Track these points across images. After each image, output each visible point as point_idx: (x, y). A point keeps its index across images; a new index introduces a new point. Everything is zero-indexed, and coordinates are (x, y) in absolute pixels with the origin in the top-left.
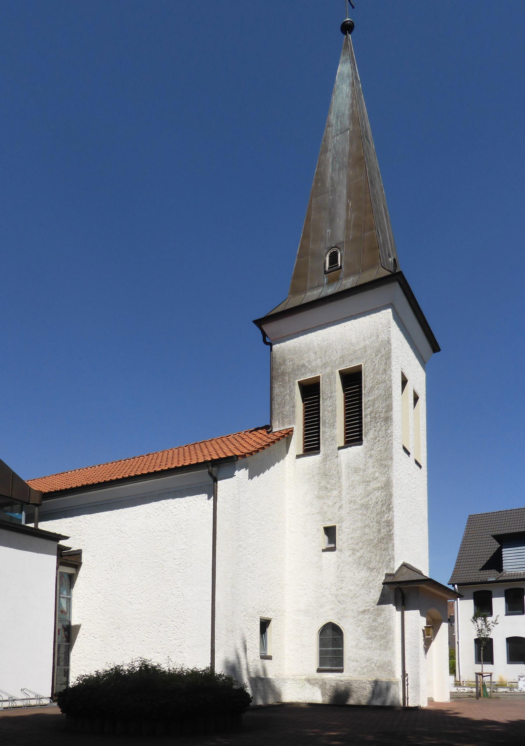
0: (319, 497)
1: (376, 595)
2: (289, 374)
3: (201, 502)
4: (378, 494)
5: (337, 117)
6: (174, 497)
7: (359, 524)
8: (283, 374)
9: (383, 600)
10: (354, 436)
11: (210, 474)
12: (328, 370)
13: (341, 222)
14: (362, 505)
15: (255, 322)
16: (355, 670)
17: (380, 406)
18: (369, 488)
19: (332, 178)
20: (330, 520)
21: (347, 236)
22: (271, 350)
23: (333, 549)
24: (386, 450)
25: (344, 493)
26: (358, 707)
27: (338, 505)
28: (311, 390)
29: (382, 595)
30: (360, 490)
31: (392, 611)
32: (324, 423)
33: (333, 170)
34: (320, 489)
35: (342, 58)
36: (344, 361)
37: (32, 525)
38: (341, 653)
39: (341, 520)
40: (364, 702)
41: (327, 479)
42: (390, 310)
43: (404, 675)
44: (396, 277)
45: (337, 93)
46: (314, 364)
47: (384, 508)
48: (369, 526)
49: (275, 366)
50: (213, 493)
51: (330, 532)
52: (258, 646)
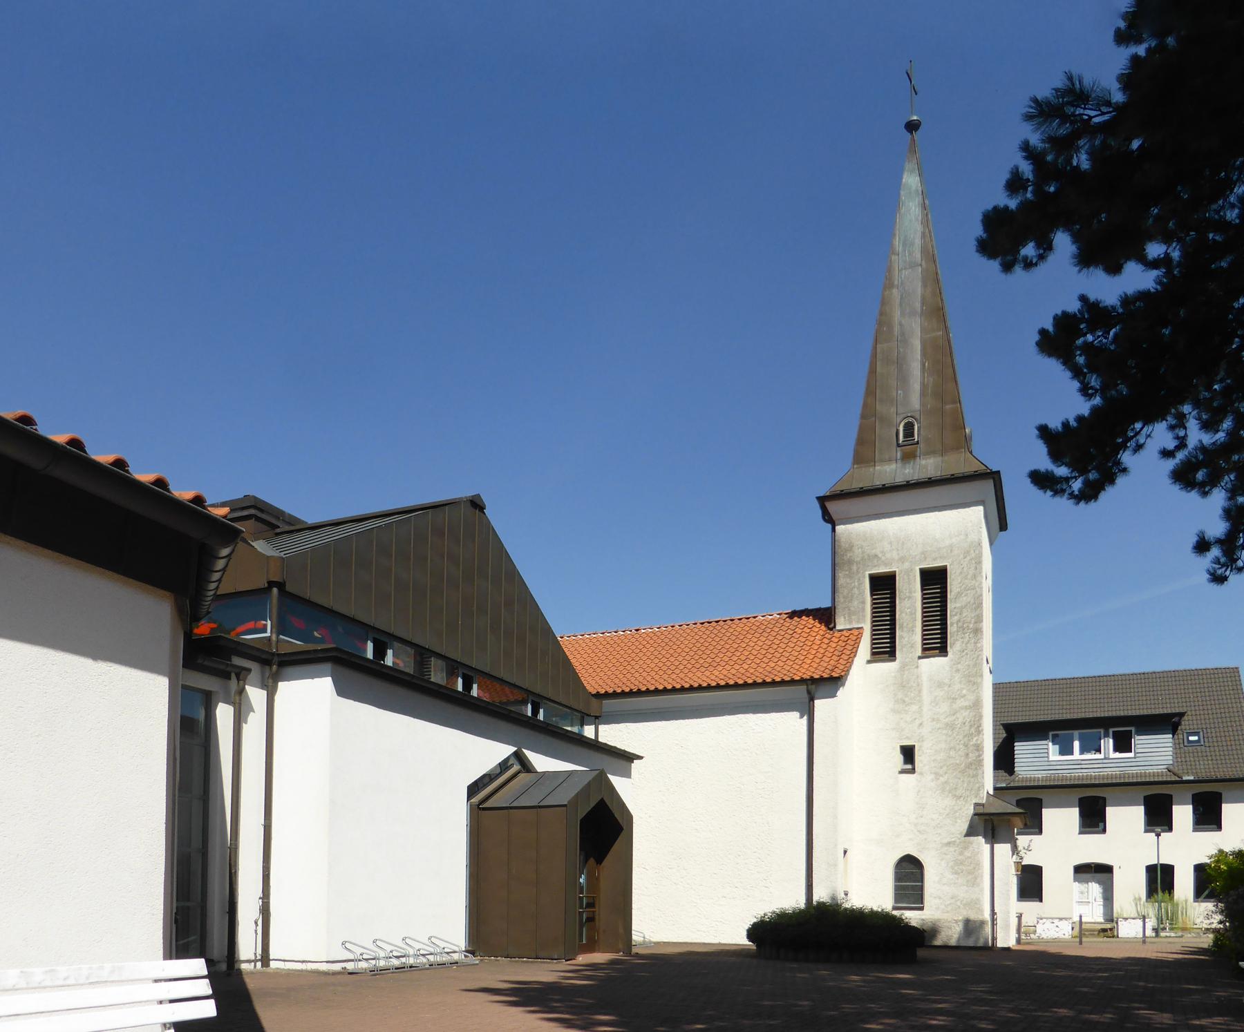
0: (894, 711)
1: (964, 826)
2: (858, 563)
3: (793, 722)
4: (965, 713)
5: (904, 244)
6: (754, 712)
7: (943, 746)
8: (850, 562)
9: (971, 832)
10: (936, 643)
11: (809, 692)
13: (916, 387)
14: (947, 724)
15: (819, 498)
16: (938, 908)
17: (968, 615)
18: (955, 706)
19: (901, 324)
21: (923, 404)
22: (834, 530)
23: (913, 771)
24: (975, 665)
25: (925, 709)
26: (946, 947)
27: (917, 722)
28: (884, 585)
30: (944, 708)
32: (901, 627)
33: (903, 314)
34: (897, 701)
35: (908, 166)
36: (925, 558)
37: (575, 729)
38: (922, 888)
39: (922, 740)
40: (953, 942)
41: (905, 691)
42: (981, 508)
43: (993, 913)
44: (995, 476)
45: (903, 211)
46: (888, 555)
47: (973, 730)
50: (1158, 835)
51: (908, 753)
52: (1100, 901)
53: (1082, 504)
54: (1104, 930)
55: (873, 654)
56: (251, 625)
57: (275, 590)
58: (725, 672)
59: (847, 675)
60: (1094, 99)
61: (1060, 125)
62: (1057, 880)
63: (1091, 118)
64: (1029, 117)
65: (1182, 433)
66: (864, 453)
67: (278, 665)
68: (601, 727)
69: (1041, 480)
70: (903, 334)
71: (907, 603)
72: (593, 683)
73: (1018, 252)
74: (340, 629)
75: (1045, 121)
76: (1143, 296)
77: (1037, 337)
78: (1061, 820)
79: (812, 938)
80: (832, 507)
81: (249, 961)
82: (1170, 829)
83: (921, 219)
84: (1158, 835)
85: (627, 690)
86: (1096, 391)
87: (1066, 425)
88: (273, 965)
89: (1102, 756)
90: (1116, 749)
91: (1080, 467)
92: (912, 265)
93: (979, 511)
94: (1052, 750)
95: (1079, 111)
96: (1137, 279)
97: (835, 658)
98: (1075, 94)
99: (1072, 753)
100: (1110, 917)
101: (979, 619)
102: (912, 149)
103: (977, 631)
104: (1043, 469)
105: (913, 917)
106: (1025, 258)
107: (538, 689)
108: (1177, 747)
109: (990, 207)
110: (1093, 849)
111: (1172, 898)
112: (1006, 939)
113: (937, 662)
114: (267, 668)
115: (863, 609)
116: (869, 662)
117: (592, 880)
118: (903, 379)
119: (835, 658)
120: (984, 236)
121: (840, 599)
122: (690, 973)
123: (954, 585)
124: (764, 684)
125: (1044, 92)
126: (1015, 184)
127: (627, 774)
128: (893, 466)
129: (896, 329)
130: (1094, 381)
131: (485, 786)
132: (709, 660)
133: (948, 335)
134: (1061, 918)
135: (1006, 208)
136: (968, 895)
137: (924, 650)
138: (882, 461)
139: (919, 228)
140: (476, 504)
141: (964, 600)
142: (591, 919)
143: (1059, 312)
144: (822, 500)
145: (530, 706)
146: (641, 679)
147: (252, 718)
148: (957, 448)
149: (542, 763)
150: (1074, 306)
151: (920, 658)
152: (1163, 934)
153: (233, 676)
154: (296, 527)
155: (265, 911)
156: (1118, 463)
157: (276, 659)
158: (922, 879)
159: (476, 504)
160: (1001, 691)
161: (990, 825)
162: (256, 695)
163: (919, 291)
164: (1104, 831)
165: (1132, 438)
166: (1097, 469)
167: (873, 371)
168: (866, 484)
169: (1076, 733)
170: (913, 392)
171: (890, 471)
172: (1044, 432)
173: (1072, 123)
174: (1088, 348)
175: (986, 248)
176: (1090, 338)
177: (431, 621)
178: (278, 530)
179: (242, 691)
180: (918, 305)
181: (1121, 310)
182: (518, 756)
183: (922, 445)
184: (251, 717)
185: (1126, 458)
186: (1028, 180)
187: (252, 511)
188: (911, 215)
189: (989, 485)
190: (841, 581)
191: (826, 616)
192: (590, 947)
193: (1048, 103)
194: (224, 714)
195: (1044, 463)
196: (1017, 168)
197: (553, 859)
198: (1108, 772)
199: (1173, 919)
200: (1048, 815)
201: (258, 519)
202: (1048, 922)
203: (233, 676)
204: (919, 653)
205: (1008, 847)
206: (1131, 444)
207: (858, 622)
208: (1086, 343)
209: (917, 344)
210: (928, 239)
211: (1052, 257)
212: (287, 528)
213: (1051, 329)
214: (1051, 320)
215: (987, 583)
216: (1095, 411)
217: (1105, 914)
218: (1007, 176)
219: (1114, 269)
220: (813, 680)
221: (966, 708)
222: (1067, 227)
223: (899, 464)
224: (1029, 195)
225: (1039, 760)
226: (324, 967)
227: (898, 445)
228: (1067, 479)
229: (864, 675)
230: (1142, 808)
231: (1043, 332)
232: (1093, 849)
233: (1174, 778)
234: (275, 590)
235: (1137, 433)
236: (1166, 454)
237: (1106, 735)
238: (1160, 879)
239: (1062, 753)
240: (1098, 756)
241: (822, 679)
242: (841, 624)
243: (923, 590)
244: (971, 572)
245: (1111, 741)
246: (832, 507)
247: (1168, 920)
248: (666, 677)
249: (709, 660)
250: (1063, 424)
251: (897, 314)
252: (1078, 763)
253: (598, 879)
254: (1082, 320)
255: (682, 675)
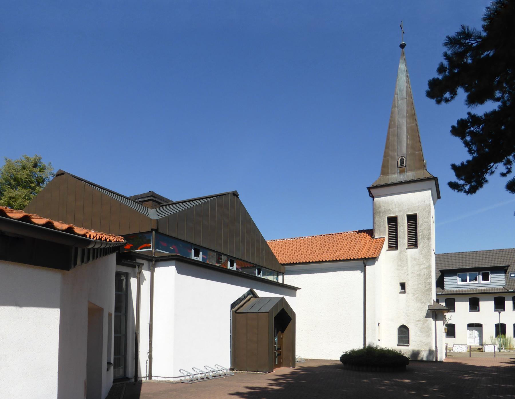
1: (425, 314)
2: (383, 213)
3: (358, 275)
5: (400, 91)
6: (343, 271)
7: (416, 283)
8: (380, 212)
9: (427, 316)
10: (413, 243)
11: (364, 263)
12: (401, 213)
13: (405, 144)
15: (367, 188)
17: (426, 232)
18: (421, 268)
19: (399, 121)
20: (402, 280)
21: (407, 151)
22: (373, 200)
23: (405, 292)
24: (428, 252)
27: (406, 274)
29: (427, 314)
30: (417, 268)
31: (431, 320)
32: (400, 237)
33: (399, 117)
35: (401, 61)
38: (408, 338)
39: (408, 280)
41: (402, 262)
42: (430, 191)
43: (436, 348)
44: (435, 179)
46: (394, 210)
47: (428, 277)
48: (420, 284)
49: (375, 208)
50: (500, 313)
51: (403, 286)
52: (478, 338)
53: (469, 195)
54: (479, 349)
55: (389, 247)
56: (145, 245)
57: (154, 232)
58: (332, 255)
59: (378, 257)
60: (474, 36)
61: (459, 48)
62: (461, 329)
63: (472, 44)
64: (446, 45)
65: (509, 167)
66: (385, 170)
67: (155, 261)
68: (285, 276)
69: (453, 186)
70: (399, 125)
71: (402, 228)
72: (282, 259)
73: (443, 96)
74: (181, 245)
75: (452, 46)
76: (494, 112)
77: (451, 129)
78: (462, 307)
79: (366, 362)
80: (373, 191)
81: (144, 377)
82: (504, 310)
83: (406, 82)
84: (500, 313)
85: (295, 262)
86: (475, 151)
87: (462, 164)
88: (153, 378)
89: (477, 282)
90: (483, 279)
91: (468, 181)
92: (403, 99)
93: (429, 192)
94: (459, 280)
95: (467, 41)
96: (490, 106)
97: (374, 249)
98: (465, 34)
99: (466, 281)
100: (481, 344)
101: (430, 234)
102: (403, 55)
103: (429, 239)
104: (453, 181)
105: (406, 351)
106: (446, 98)
107: (260, 264)
108: (506, 279)
109: (431, 78)
110: (474, 317)
111: (505, 337)
112: (441, 357)
113: (414, 251)
114: (151, 263)
115: (385, 230)
116: (387, 250)
117: (280, 340)
118: (400, 142)
119: (374, 249)
120: (429, 90)
121: (376, 227)
122: (318, 376)
123: (420, 221)
124: (347, 260)
125: (452, 34)
126: (441, 69)
127: (295, 295)
128: (396, 175)
129: (397, 122)
130: (474, 148)
131: (238, 304)
132: (326, 250)
133: (417, 124)
134: (464, 342)
135: (438, 78)
136: (428, 341)
137: (409, 246)
138: (392, 173)
139: (405, 84)
140: (235, 194)
141: (424, 227)
142: (279, 354)
143: (460, 119)
144: (369, 189)
145: (257, 271)
146: (300, 258)
147: (145, 283)
148: (420, 168)
149: (261, 294)
150: (465, 117)
151: (407, 249)
152: (502, 351)
153: (137, 266)
154: (168, 203)
155: (150, 357)
156: (484, 179)
157: (154, 259)
158: (408, 334)
159: (235, 194)
160: (439, 257)
161: (435, 314)
162: (146, 274)
163: (406, 108)
164: (479, 311)
165: (489, 169)
166: (476, 181)
167: (388, 139)
168: (385, 182)
169: (468, 273)
170: (403, 147)
171: (395, 177)
172: (454, 167)
173: (464, 46)
174: (471, 133)
175: (430, 95)
176: (472, 129)
177: (217, 241)
178: (161, 205)
179: (140, 272)
180: (405, 114)
181: (484, 118)
182: (251, 292)
183: (407, 167)
184: (145, 282)
185: (487, 177)
186: (446, 68)
187: (152, 198)
188: (402, 80)
189: (433, 182)
190: (377, 219)
191: (371, 233)
192: (279, 365)
193: (454, 38)
194: (133, 282)
195: (454, 179)
196: (442, 63)
197: (264, 331)
198: (481, 288)
199: (505, 345)
200: (458, 305)
201: (153, 201)
202: (458, 346)
203: (137, 266)
204: (407, 247)
205: (442, 322)
206: (489, 171)
207: (383, 235)
208: (470, 131)
209: (405, 129)
210: (409, 88)
211: (456, 98)
212: (165, 204)
213: (456, 126)
214: (456, 122)
215: (433, 220)
216: (474, 158)
217: (479, 343)
218: (438, 66)
219: (482, 102)
220: (365, 259)
221: (425, 268)
222: (462, 86)
223: (398, 175)
224: (447, 74)
225: (453, 284)
226: (172, 380)
227: (398, 167)
228: (463, 185)
229: (386, 255)
230: (493, 302)
231: (453, 127)
232: (474, 317)
233: (506, 291)
234: (154, 232)
235: (491, 167)
236: (503, 175)
237: (479, 274)
238: (500, 329)
239: (463, 281)
240: (476, 282)
241: (369, 258)
242: (377, 236)
243: (408, 223)
244: (427, 216)
245: (481, 276)
246: (373, 191)
247: (503, 345)
248: (310, 257)
249: (326, 250)
250: (461, 163)
251: (397, 116)
252: (469, 285)
253: (282, 338)
254: (469, 122)
255: (316, 256)
